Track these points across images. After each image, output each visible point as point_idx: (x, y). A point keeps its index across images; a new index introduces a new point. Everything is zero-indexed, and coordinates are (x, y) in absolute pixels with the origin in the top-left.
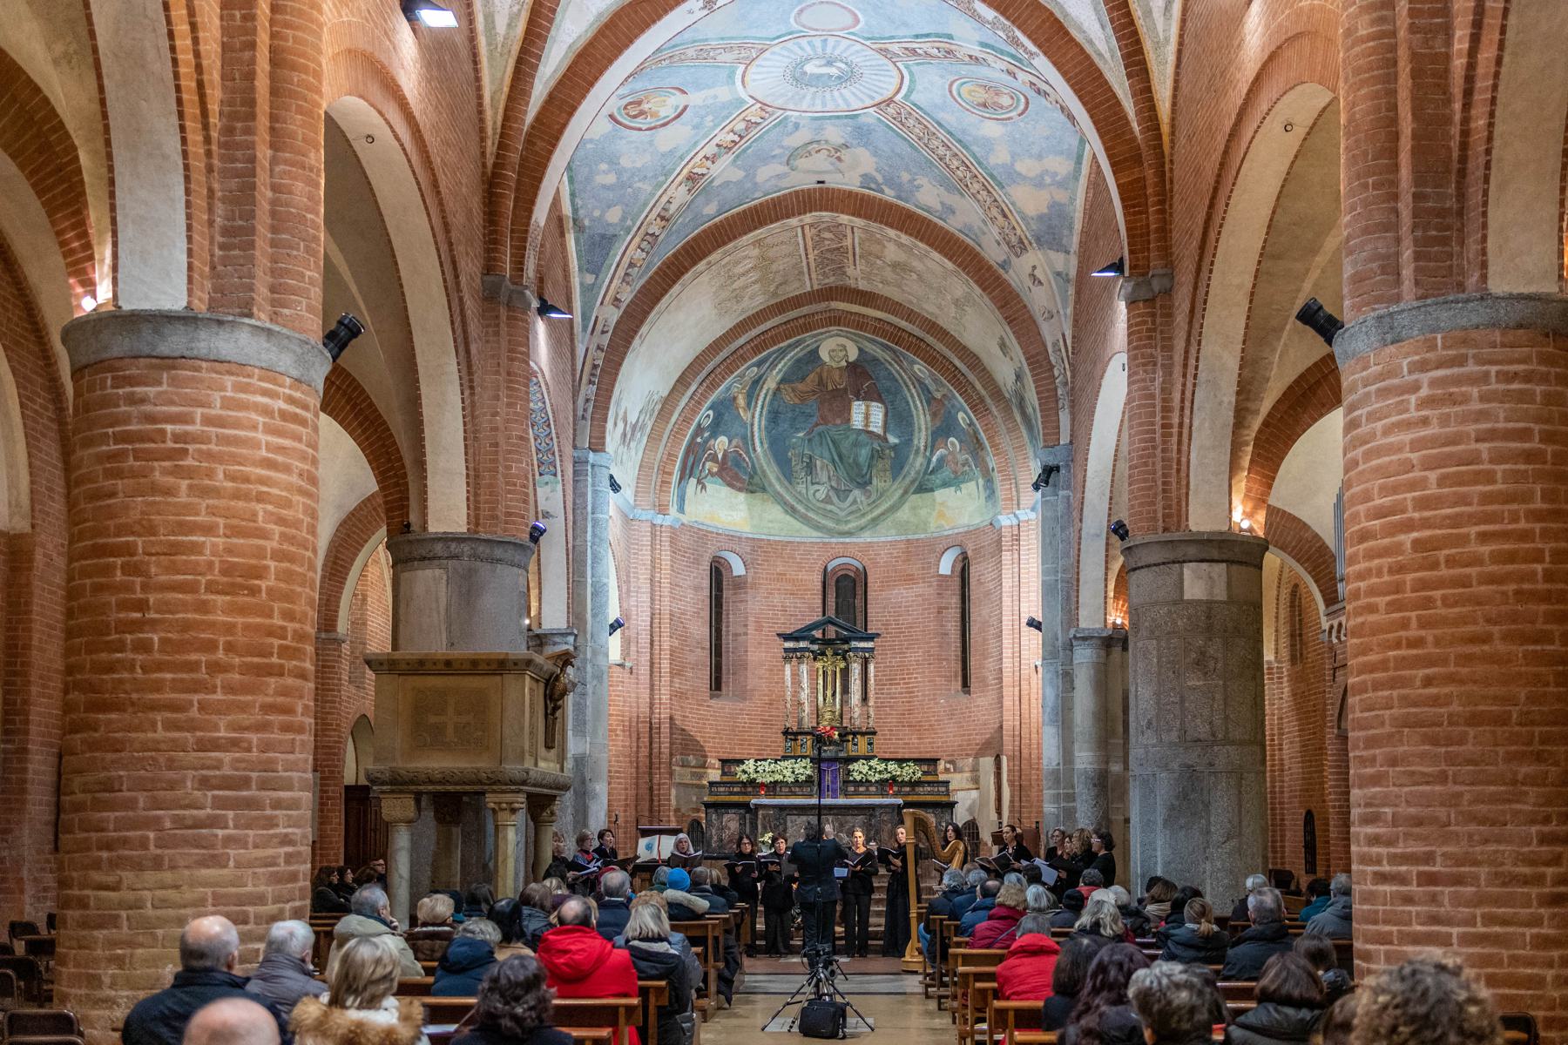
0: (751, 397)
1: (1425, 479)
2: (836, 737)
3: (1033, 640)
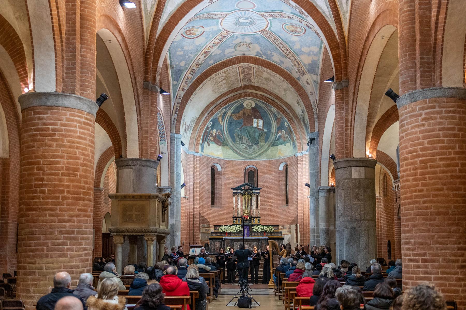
0: (223, 118)
1: (424, 142)
2: (249, 219)
3: (307, 190)
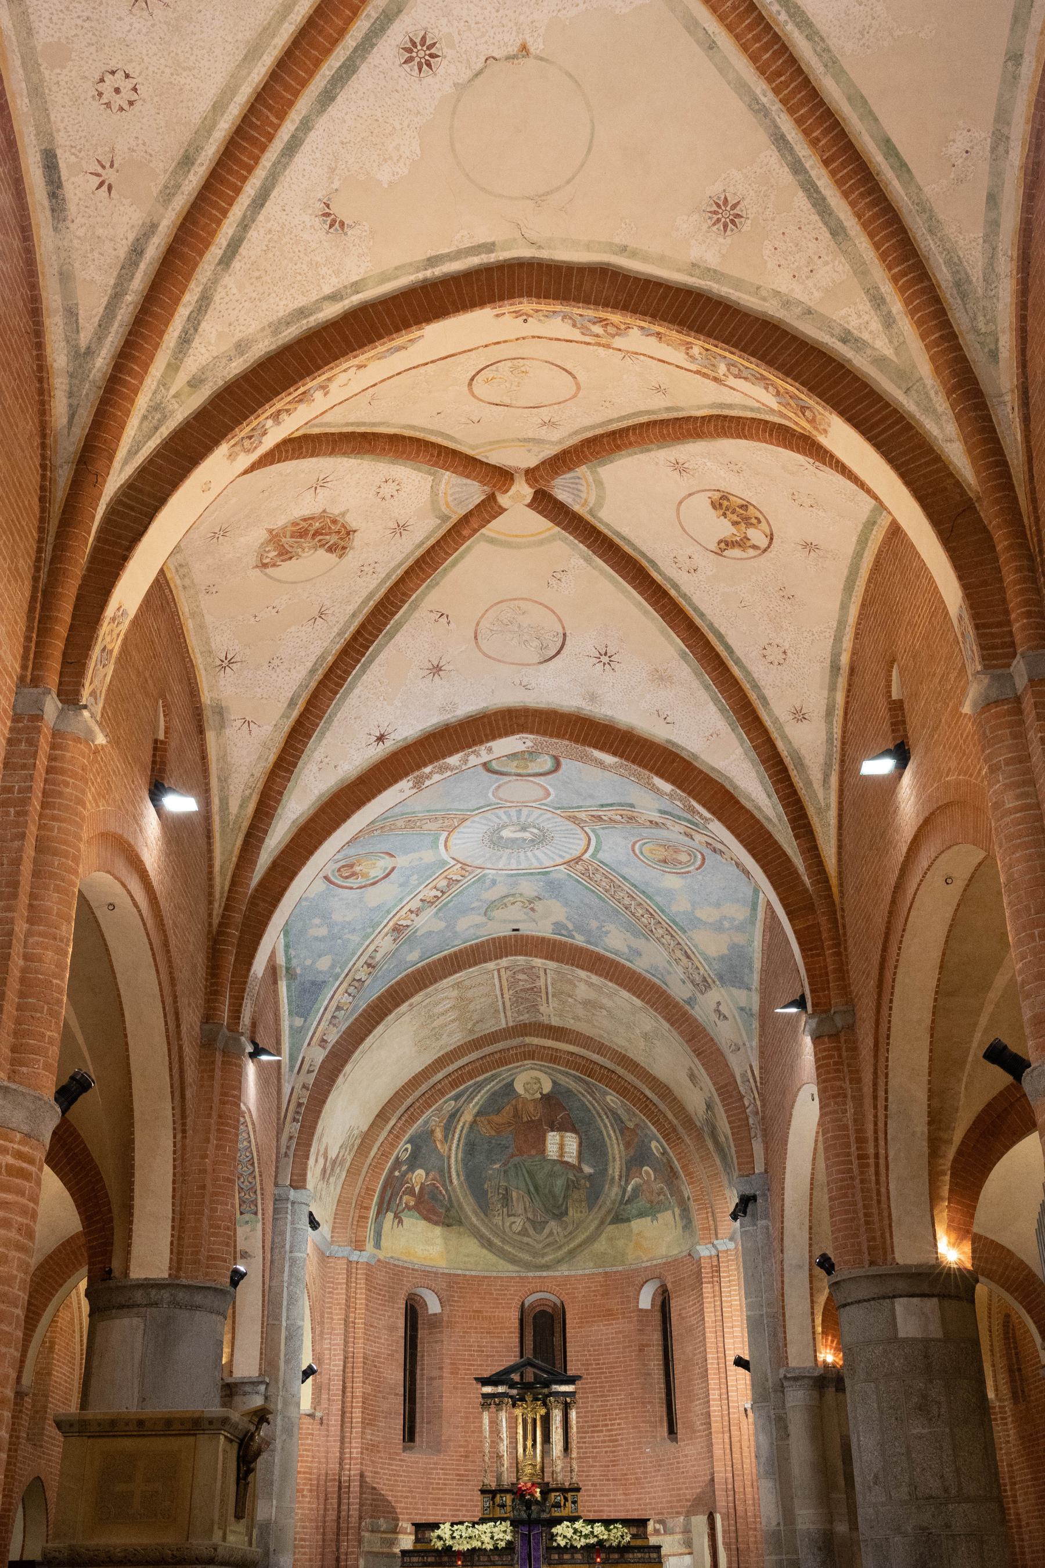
0: (448, 1129)
2: (538, 1495)
3: (741, 1379)
